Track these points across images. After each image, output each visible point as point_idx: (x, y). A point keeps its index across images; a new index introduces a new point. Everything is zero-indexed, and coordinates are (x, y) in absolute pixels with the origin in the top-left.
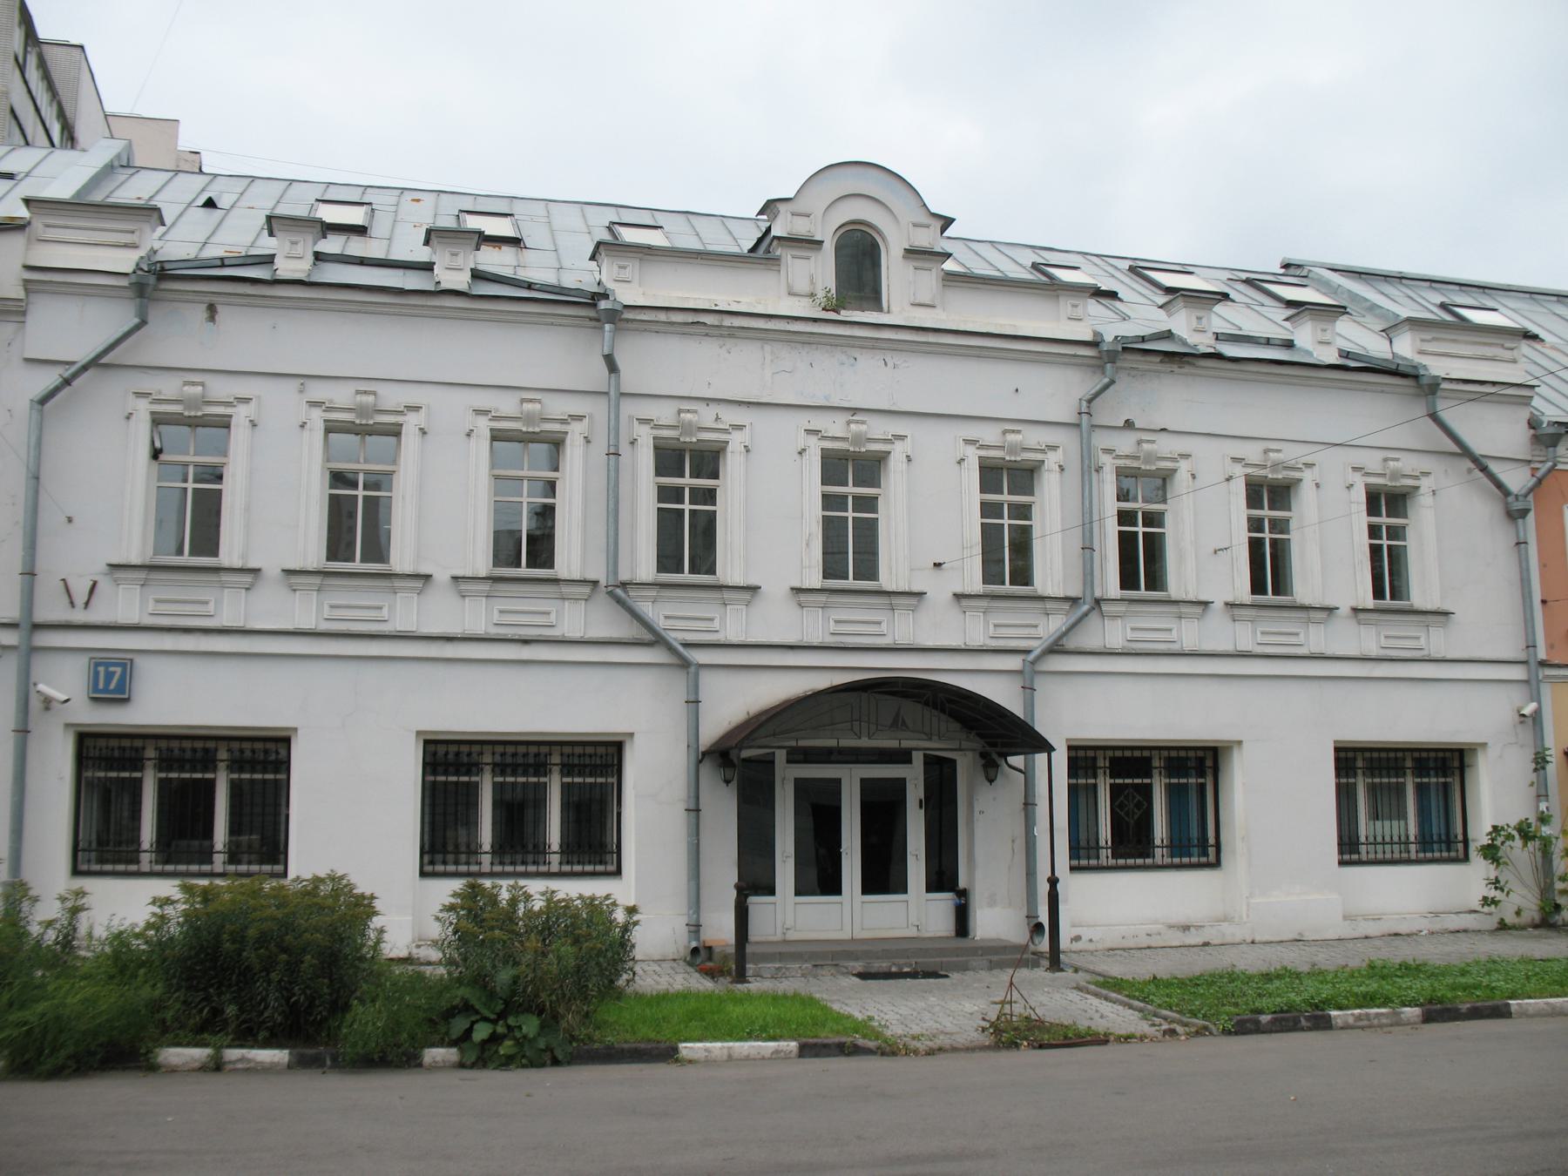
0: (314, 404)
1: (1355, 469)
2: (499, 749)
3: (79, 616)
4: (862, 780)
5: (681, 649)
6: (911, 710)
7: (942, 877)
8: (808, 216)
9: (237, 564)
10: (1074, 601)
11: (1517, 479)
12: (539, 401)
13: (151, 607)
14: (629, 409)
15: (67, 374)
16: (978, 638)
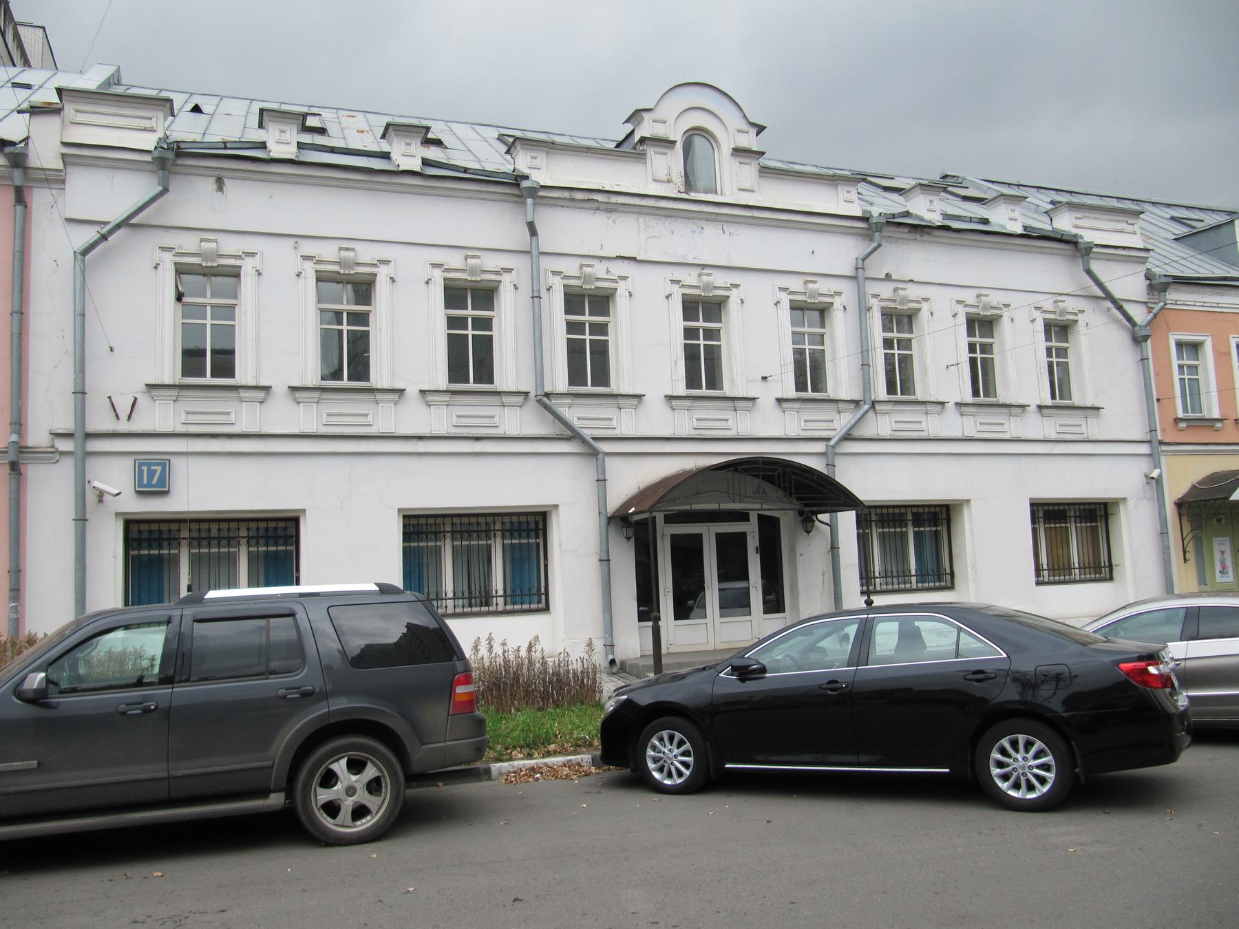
0: (306, 258)
1: (1037, 308)
2: (253, 525)
3: (123, 426)
4: (717, 534)
5: (592, 442)
6: (752, 483)
7: (774, 604)
8: (664, 122)
9: (251, 383)
10: (856, 403)
11: (1139, 315)
12: (215, 241)
13: (183, 418)
14: (547, 264)
15: (104, 231)
16: (794, 431)
